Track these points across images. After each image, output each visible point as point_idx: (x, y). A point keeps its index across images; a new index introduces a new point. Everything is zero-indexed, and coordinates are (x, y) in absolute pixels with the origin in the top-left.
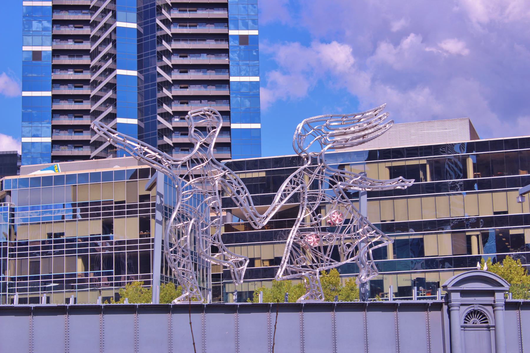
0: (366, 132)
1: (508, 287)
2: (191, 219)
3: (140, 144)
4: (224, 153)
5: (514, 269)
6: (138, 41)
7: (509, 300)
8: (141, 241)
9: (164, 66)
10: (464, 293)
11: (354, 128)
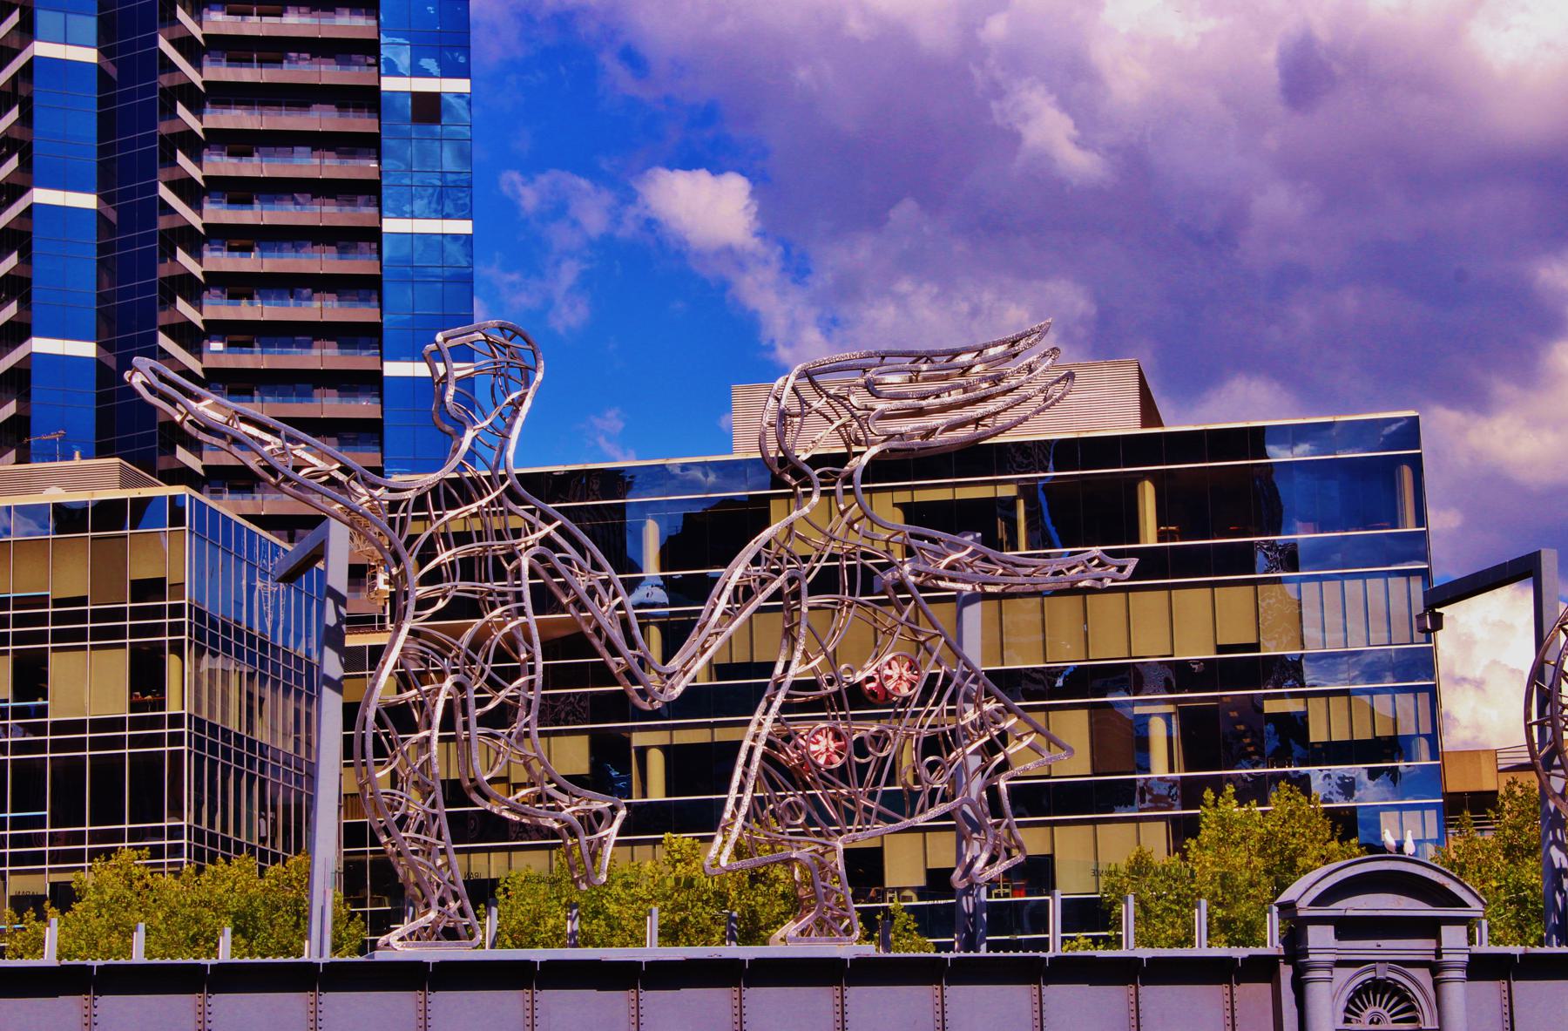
0: (990, 406)
1: (1479, 907)
2: (441, 676)
3: (283, 433)
4: (362, 451)
5: (1304, 822)
6: (102, 103)
7: (1485, 947)
8: (136, 723)
9: (181, 181)
10: (1348, 928)
11: (950, 395)
